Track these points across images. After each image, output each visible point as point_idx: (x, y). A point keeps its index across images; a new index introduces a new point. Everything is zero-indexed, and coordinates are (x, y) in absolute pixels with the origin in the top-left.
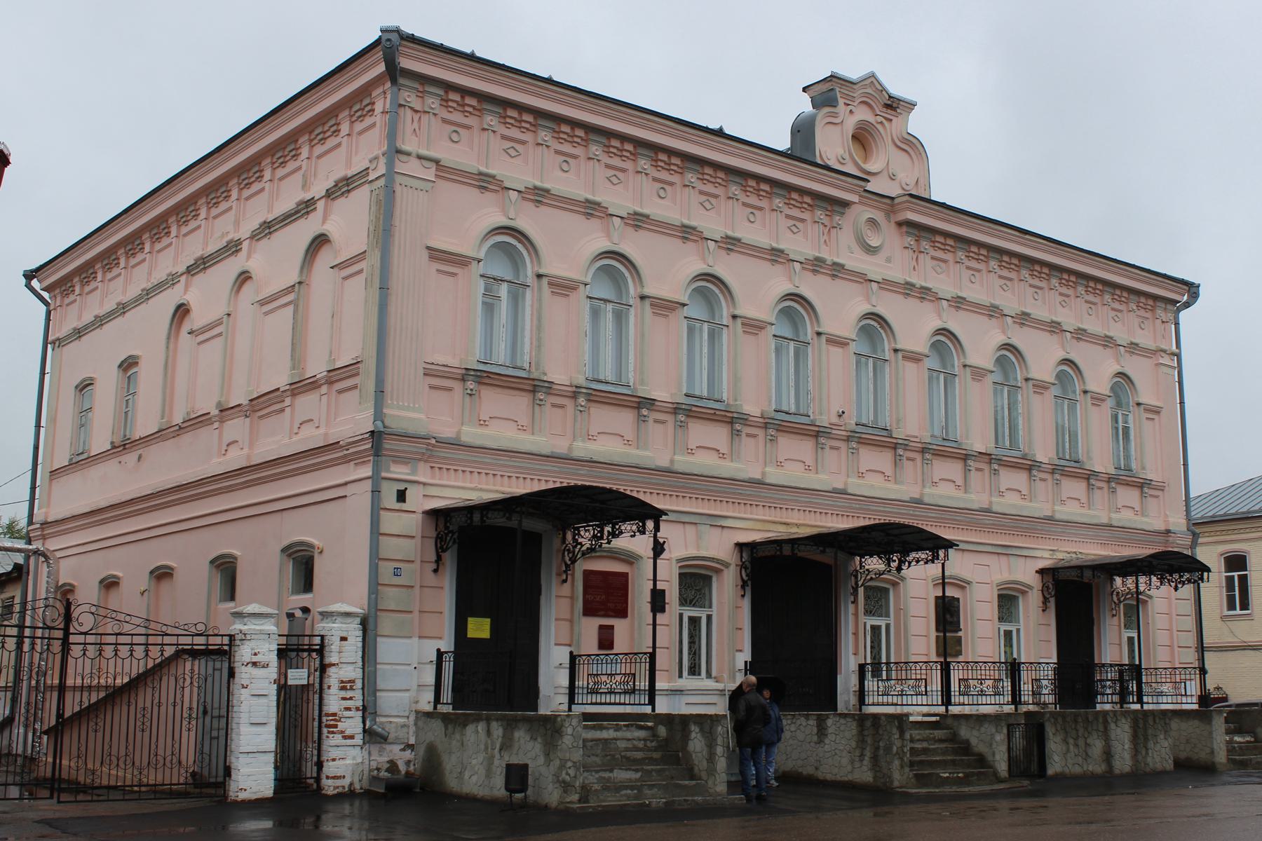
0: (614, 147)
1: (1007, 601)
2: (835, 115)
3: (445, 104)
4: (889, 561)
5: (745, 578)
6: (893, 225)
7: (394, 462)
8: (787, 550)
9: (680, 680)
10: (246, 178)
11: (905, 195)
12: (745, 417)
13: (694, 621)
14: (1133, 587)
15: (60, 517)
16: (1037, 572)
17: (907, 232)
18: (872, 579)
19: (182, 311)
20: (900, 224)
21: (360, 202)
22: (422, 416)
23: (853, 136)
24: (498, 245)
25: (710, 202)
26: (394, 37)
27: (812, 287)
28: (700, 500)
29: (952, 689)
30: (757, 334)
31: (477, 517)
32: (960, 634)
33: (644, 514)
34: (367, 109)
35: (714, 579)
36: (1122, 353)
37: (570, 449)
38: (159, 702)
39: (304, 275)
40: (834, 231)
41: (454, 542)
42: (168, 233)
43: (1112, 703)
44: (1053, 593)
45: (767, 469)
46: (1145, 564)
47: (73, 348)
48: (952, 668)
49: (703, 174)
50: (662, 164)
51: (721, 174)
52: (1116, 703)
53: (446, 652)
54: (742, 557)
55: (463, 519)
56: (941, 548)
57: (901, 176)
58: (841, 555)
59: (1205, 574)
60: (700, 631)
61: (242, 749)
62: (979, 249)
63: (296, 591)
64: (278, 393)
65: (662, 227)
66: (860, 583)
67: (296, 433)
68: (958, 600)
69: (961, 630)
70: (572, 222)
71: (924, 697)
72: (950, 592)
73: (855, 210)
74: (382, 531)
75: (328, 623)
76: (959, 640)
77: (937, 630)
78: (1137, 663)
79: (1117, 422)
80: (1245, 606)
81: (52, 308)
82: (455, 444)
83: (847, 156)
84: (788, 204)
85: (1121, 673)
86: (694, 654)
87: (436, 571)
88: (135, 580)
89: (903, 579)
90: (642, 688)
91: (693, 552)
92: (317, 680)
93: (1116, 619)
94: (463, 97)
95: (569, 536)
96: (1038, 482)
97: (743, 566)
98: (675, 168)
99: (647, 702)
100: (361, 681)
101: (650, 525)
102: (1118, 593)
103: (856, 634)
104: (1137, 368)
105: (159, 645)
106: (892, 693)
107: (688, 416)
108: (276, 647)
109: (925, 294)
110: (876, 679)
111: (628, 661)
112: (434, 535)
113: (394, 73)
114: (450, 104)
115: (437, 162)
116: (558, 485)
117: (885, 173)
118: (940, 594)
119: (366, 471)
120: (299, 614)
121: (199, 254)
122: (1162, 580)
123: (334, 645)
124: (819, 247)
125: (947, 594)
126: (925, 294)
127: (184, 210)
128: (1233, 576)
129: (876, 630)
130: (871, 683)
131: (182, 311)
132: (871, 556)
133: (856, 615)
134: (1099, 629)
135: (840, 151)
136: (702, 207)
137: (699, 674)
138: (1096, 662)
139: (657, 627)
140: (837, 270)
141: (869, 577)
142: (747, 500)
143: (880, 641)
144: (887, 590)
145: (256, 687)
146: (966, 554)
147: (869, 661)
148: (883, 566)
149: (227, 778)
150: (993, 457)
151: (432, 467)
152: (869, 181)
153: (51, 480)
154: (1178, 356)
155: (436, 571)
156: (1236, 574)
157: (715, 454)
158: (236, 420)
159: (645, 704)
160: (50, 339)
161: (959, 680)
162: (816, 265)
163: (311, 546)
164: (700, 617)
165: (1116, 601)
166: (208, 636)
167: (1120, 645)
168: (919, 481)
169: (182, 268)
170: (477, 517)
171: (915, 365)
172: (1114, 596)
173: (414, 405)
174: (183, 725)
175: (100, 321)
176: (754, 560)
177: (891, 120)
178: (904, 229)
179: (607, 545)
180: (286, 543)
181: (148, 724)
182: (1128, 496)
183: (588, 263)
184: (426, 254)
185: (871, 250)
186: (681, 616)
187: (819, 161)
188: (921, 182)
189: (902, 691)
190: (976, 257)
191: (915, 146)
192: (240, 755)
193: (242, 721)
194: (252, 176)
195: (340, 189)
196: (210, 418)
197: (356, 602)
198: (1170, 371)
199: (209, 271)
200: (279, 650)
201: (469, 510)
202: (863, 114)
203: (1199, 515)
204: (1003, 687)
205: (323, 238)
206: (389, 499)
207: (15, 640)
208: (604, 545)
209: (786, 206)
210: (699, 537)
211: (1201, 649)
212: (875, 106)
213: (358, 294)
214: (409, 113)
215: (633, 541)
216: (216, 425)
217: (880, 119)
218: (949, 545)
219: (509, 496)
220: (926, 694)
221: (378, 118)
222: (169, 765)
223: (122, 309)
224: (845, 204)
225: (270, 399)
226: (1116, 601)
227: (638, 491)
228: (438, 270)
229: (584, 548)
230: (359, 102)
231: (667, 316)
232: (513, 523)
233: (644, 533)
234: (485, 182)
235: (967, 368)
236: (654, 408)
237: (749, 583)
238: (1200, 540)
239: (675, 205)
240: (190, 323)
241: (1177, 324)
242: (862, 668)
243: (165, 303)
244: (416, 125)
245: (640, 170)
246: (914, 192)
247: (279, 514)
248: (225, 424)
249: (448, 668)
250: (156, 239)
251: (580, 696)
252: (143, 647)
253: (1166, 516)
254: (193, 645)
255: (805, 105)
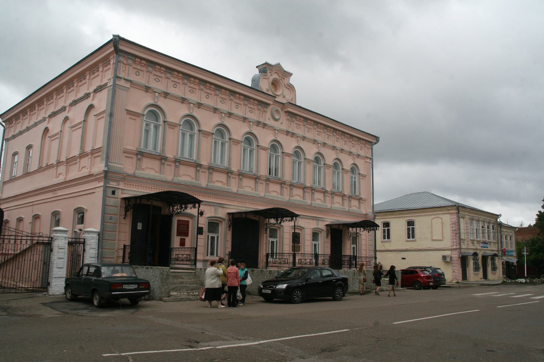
0: (192, 81)
1: (315, 235)
2: (266, 76)
3: (134, 62)
4: (277, 221)
5: (230, 224)
6: (284, 113)
7: (111, 181)
8: (244, 216)
9: (207, 257)
10: (69, 86)
11: (287, 103)
12: (232, 172)
13: (213, 238)
14: (355, 231)
15: (5, 198)
16: (325, 225)
17: (288, 115)
18: (272, 226)
19: (46, 130)
20: (286, 112)
21: (104, 95)
22: (122, 166)
23: (272, 83)
24: (151, 111)
25: (224, 101)
26: (117, 38)
27: (256, 131)
28: (203, 196)
29: (296, 262)
30: (207, 137)
31: (138, 200)
32: (300, 244)
33: (196, 202)
34: (108, 63)
35: (220, 224)
36: (299, 139)
37: (173, 179)
38: (25, 259)
39: (86, 119)
40: (264, 113)
41: (131, 209)
42: (43, 104)
43: (347, 267)
44: (330, 232)
45: (239, 189)
46: (359, 224)
47: (12, 142)
48: (296, 255)
49: (173, 75)
50: (208, 87)
51: (227, 92)
52: (348, 267)
53: (127, 246)
54: (229, 217)
55: (134, 201)
56: (190, 203)
57: (287, 97)
58: (261, 218)
59: (378, 228)
60: (214, 241)
61: (53, 276)
62: (210, 85)
63: (79, 224)
64: (75, 158)
65: (237, 117)
66: (268, 227)
67: (81, 171)
68: (300, 233)
69: (300, 243)
70: (239, 123)
71: (287, 265)
72: (297, 231)
73: (271, 106)
74: (106, 204)
75: (87, 234)
76: (299, 247)
77: (293, 243)
78: (355, 255)
79: (352, 179)
80: (389, 238)
81: (5, 128)
82: (134, 176)
83: (269, 89)
84: (249, 103)
85: (350, 258)
86: (212, 248)
87: (124, 218)
88: (28, 219)
89: (282, 226)
90: (192, 259)
91: (213, 215)
92: (82, 253)
93: (349, 241)
94: (141, 60)
95: (171, 208)
96: (327, 197)
97: (229, 220)
98: (212, 89)
99: (194, 264)
100: (97, 254)
101: (197, 205)
102: (350, 233)
103: (266, 244)
104: (360, 162)
105: (26, 240)
106: (277, 263)
107: (243, 176)
108: (67, 242)
109: (293, 135)
110: (272, 258)
111: (188, 250)
112: (124, 206)
113: (117, 51)
114: (136, 62)
115: (131, 81)
116: (163, 191)
117: (282, 95)
118: (294, 232)
119: (102, 184)
120: (78, 231)
121: (52, 111)
122: (364, 229)
123: (88, 242)
124: (259, 118)
125: (296, 232)
126: (293, 135)
127: (49, 96)
128: (385, 229)
129: (273, 242)
130: (270, 260)
131: (46, 130)
132: (271, 219)
133: (266, 237)
134: (344, 244)
135: (267, 87)
136: (190, 92)
137: (214, 255)
138: (343, 254)
139: (198, 239)
140: (265, 125)
141: (271, 225)
142: (162, 188)
143: (274, 246)
144: (277, 230)
145: (61, 255)
146: (303, 219)
147: (270, 252)
148: (276, 222)
149: (48, 286)
150: (313, 188)
151: (125, 184)
152: (276, 97)
153: (3, 185)
154: (372, 159)
155: (124, 218)
156: (386, 228)
157: (221, 183)
158: (62, 166)
159: (193, 265)
160: (5, 138)
161: (299, 259)
162: (258, 123)
163: (83, 208)
164: (215, 237)
165: (350, 235)
166: (44, 237)
167: (350, 249)
168: (330, 203)
169: (47, 116)
170: (138, 200)
171: (289, 158)
172: (349, 234)
173: (119, 162)
174: (33, 268)
175: (21, 133)
176: (233, 219)
177: (284, 79)
178: (287, 114)
179: (183, 212)
180: (76, 207)
181: (37, 267)
182: (355, 203)
183: (214, 126)
184: (125, 112)
185: (276, 120)
186: (208, 236)
187: (260, 90)
188: (293, 99)
189: (280, 262)
190: (310, 124)
191: (292, 87)
192: (53, 278)
193: (54, 267)
194: (71, 85)
195: (98, 89)
196: (54, 166)
197: (97, 228)
198: (369, 164)
199: (56, 116)
200: (69, 243)
201: (136, 198)
202: (275, 76)
203: (376, 210)
204: (312, 262)
205: (93, 106)
206: (109, 194)
207: (14, 240)
208: (182, 212)
209: (249, 104)
210: (215, 211)
211: (375, 251)
212: (279, 73)
213: (102, 124)
214: (122, 65)
215: (192, 211)
216: (55, 168)
217: (281, 78)
218: (297, 216)
219: (148, 194)
220: (288, 264)
221: (111, 66)
222: (27, 281)
223: (28, 129)
224: (268, 105)
225: (73, 159)
226: (350, 235)
227: (195, 195)
228: (130, 118)
229: (176, 212)
230: (105, 61)
231: (135, 120)
232: (150, 203)
233: (195, 208)
234: (147, 89)
235: (306, 160)
236: (260, 179)
237: (231, 226)
238: (376, 218)
239: (143, 78)
240: (49, 134)
241: (372, 149)
242: (267, 255)
243: (41, 128)
244: (124, 69)
245: (148, 71)
246: (291, 102)
247: (74, 198)
248: (58, 168)
249: (128, 250)
250: (40, 106)
251: (173, 261)
252: (14, 240)
253: (366, 209)
254: (43, 240)
255: (257, 72)
